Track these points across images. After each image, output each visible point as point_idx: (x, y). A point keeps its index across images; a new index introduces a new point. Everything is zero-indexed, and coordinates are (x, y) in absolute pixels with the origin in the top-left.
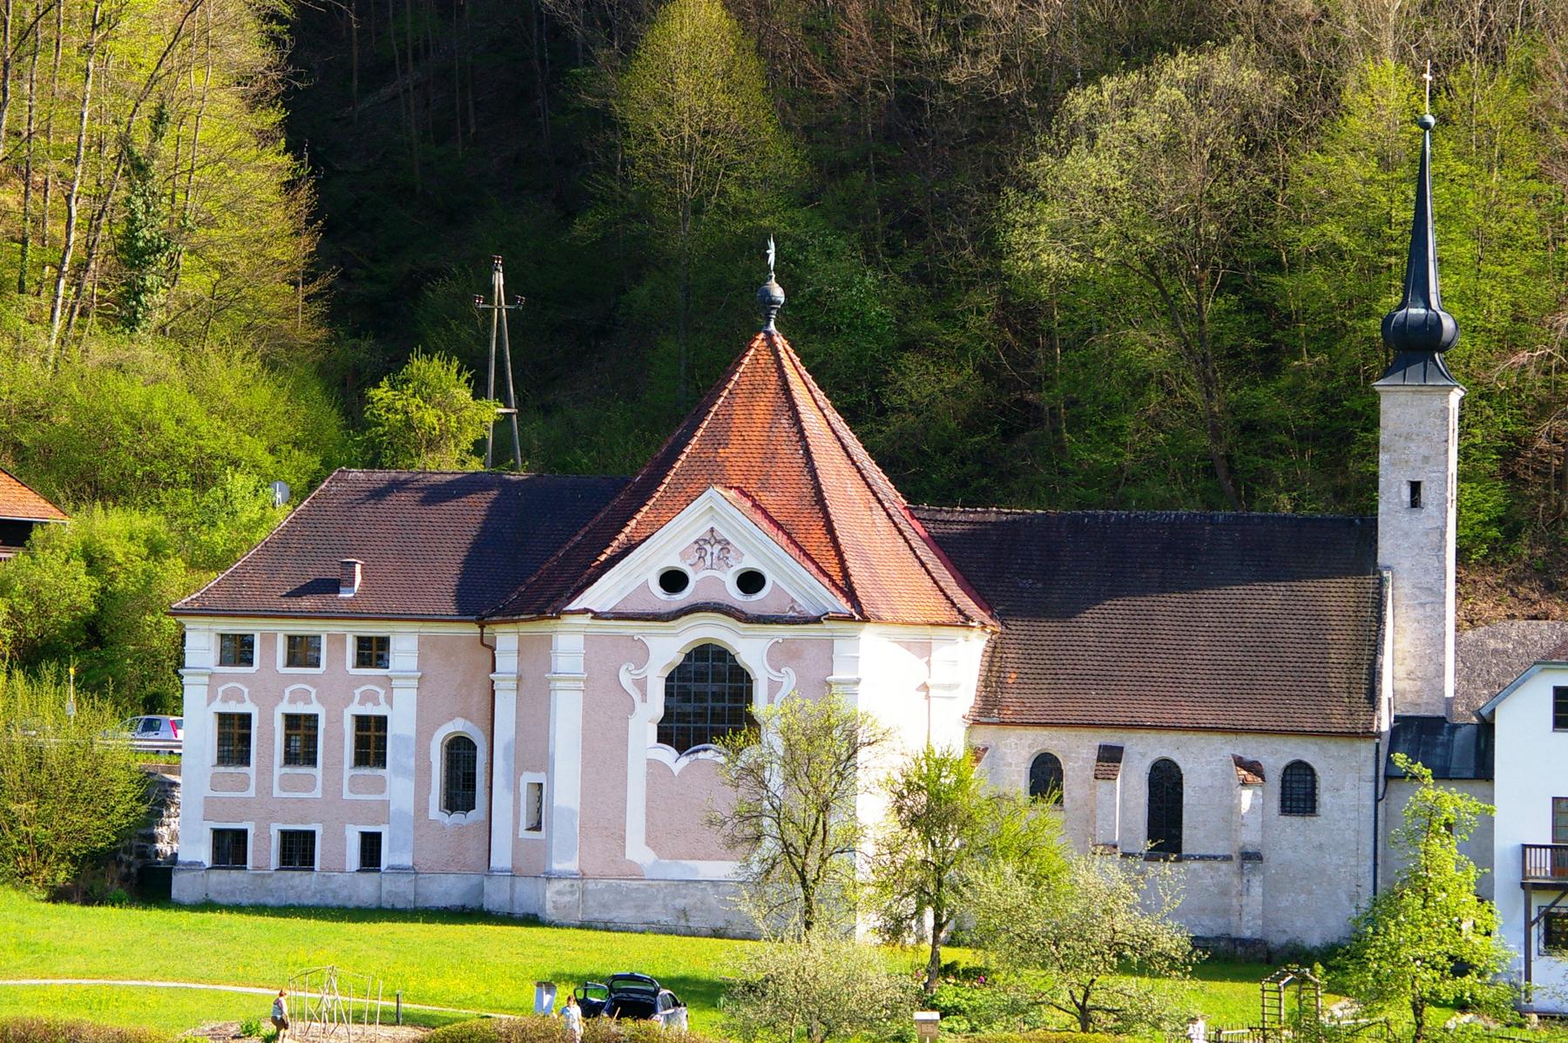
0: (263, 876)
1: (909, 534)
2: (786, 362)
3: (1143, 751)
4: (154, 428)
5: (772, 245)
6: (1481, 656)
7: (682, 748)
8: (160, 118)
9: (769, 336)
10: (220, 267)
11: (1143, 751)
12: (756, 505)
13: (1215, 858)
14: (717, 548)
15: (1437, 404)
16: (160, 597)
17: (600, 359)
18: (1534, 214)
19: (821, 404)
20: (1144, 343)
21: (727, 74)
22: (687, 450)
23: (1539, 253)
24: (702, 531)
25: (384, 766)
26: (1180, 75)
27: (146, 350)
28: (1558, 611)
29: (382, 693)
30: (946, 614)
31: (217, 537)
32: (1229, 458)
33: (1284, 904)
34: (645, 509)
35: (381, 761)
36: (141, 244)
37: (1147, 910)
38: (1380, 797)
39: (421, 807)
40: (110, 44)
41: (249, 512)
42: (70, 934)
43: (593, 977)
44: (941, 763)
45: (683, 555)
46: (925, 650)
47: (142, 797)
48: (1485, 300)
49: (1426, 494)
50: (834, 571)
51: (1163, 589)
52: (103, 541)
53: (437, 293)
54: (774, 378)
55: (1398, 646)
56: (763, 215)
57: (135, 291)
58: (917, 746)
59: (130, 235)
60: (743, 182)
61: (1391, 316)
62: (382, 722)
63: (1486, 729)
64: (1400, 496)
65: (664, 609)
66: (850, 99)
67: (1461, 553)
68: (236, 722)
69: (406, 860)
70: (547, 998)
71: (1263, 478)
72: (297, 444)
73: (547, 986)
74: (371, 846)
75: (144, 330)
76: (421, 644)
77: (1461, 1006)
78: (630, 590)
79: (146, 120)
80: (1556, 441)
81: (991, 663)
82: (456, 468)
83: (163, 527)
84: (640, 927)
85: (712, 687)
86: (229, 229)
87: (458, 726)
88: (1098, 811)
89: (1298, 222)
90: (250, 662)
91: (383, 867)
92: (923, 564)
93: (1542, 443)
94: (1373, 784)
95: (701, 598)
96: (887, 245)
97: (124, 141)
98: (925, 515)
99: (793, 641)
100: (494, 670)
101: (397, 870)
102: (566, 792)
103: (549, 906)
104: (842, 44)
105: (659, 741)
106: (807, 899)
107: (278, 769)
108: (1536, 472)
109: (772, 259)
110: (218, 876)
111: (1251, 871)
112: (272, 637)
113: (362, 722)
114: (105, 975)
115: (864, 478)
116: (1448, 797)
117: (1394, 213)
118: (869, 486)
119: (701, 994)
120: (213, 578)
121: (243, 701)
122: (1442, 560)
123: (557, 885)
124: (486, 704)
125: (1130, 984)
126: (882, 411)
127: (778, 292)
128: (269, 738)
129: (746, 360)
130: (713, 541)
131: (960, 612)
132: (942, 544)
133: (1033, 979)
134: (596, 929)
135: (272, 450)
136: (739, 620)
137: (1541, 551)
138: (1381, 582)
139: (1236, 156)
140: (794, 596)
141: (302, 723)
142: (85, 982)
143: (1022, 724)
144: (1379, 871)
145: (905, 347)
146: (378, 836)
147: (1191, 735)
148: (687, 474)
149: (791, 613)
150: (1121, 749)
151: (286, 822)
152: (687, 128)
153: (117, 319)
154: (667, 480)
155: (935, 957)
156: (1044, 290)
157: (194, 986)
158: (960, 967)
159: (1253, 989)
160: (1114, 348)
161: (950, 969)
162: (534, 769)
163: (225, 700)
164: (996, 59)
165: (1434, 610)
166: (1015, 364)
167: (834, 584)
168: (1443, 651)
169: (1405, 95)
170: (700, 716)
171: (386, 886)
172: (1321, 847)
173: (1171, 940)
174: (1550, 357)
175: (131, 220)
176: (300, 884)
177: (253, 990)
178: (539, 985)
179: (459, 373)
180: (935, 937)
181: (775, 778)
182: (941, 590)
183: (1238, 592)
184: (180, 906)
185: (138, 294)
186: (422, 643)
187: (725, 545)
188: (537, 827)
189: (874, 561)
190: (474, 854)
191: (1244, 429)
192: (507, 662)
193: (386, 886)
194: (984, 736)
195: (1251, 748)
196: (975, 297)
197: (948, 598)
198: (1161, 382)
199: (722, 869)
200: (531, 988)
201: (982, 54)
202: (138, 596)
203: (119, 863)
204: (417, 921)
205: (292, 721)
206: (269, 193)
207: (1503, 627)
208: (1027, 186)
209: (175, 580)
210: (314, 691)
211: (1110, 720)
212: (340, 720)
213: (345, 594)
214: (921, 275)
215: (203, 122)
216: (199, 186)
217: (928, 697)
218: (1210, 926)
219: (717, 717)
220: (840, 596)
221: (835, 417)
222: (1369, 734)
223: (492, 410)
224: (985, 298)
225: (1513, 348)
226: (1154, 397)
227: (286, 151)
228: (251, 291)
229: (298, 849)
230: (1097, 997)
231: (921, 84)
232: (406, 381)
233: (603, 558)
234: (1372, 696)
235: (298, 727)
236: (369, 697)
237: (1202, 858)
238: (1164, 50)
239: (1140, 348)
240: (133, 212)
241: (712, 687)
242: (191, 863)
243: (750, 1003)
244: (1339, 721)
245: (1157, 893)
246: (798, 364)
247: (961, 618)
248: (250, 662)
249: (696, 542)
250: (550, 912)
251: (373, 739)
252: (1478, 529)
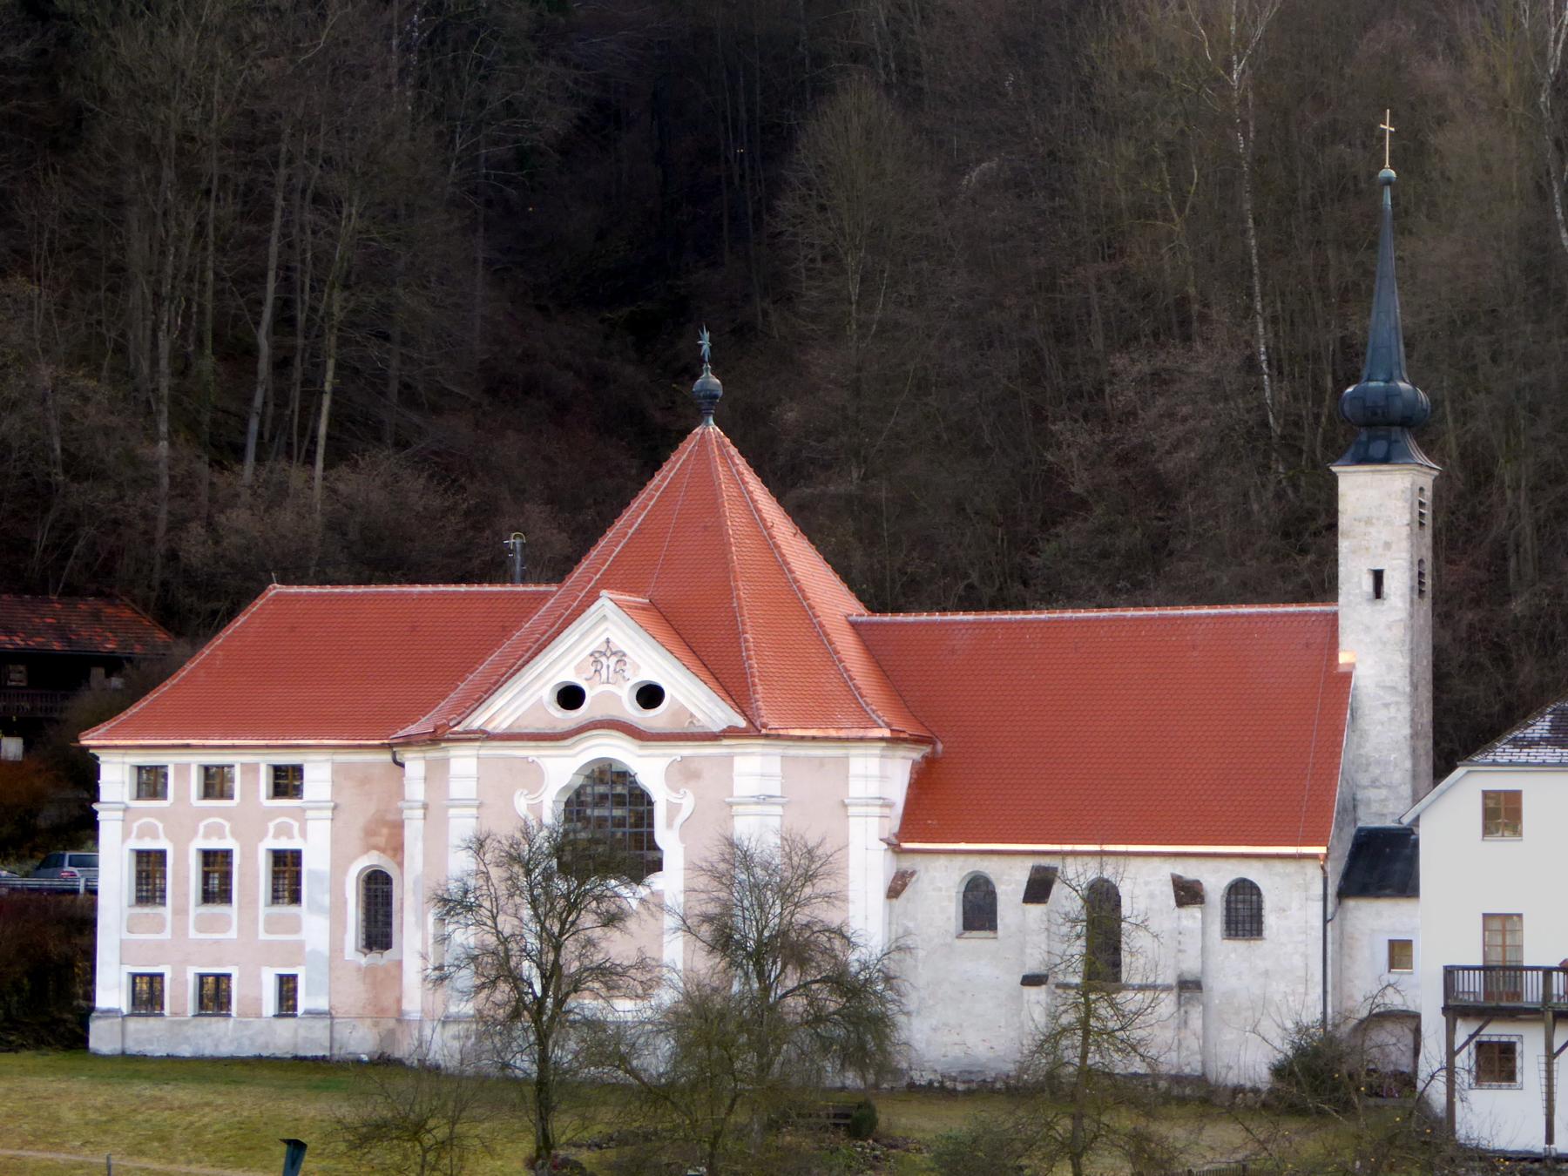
5: (707, 335)
14: (614, 659)
29: (296, 825)
38: (1329, 917)
39: (336, 948)
62: (296, 856)
64: (1360, 586)
69: (322, 1004)
74: (287, 987)
87: (372, 860)
91: (300, 1011)
94: (1321, 903)
95: (599, 714)
101: (313, 1014)
107: (195, 909)
110: (134, 1025)
128: (184, 876)
130: (608, 654)
144: (1329, 998)
151: (202, 966)
163: (140, 836)
165: (1398, 710)
172: (1266, 973)
186: (339, 771)
187: (621, 657)
193: (302, 1032)
236: (282, 831)
249: (592, 655)
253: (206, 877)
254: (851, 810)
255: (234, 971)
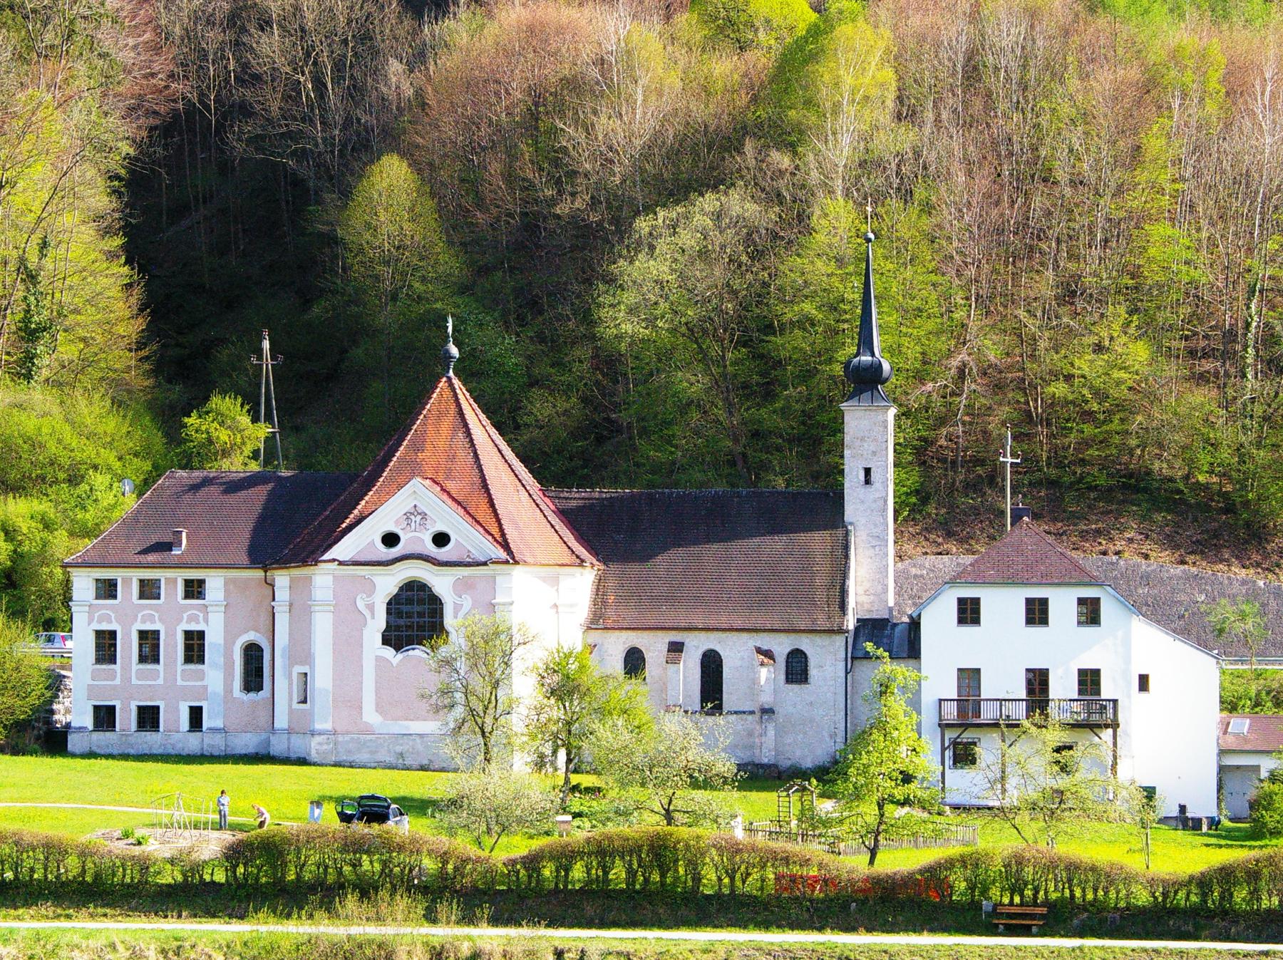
0: (127, 735)
1: (543, 507)
2: (460, 396)
3: (697, 645)
4: (42, 446)
6: (907, 579)
7: (398, 648)
8: (44, 245)
9: (449, 379)
10: (84, 340)
11: (697, 645)
12: (443, 490)
13: (744, 712)
15: (880, 418)
16: (52, 555)
17: (330, 396)
18: (934, 296)
19: (484, 423)
20: (688, 381)
21: (412, 210)
22: (398, 454)
23: (938, 320)
24: (409, 507)
25: (203, 663)
26: (708, 208)
27: (37, 395)
28: (954, 550)
30: (568, 558)
31: (88, 516)
32: (744, 455)
33: (789, 741)
34: (371, 493)
35: (201, 660)
36: (33, 326)
37: (707, 747)
40: (10, 197)
41: (107, 499)
42: (5, 774)
43: (345, 798)
44: (568, 656)
45: (397, 522)
46: (555, 581)
47: (50, 685)
48: (904, 350)
49: (874, 476)
50: (495, 531)
51: (708, 540)
52: (14, 519)
53: (224, 355)
54: (453, 407)
55: (858, 574)
56: (437, 300)
57: (30, 357)
58: (553, 646)
59: (27, 319)
60: (424, 280)
61: (849, 362)
62: (201, 635)
63: (915, 625)
65: (384, 558)
66: (491, 225)
67: (897, 513)
68: (107, 636)
70: (317, 811)
71: (764, 467)
72: (136, 455)
73: (318, 803)
74: (196, 716)
75: (36, 381)
76: (226, 584)
77: (905, 802)
78: (361, 547)
79: (35, 246)
80: (951, 440)
81: (598, 590)
82: (241, 468)
83: (52, 510)
84: (373, 765)
85: (417, 608)
86: (89, 316)
87: (251, 636)
88: (669, 684)
89: (784, 301)
90: (115, 597)
91: (204, 729)
92: (553, 526)
93: (943, 442)
95: (408, 551)
96: (518, 319)
97: (22, 260)
98: (553, 494)
99: (469, 577)
100: (274, 600)
101: (213, 730)
102: (323, 679)
103: (313, 752)
104: (485, 189)
105: (383, 644)
106: (485, 745)
108: (939, 460)
109: (450, 330)
111: (767, 720)
112: (128, 580)
113: (189, 635)
114: (30, 800)
115: (513, 471)
116: (899, 669)
117: (846, 296)
118: (516, 476)
119: (416, 807)
120: (88, 543)
121: (111, 622)
122: (885, 518)
123: (318, 739)
124: (269, 622)
125: (700, 795)
126: (517, 427)
127: (454, 351)
128: (128, 647)
129: (435, 395)
131: (578, 557)
132: (563, 514)
133: (635, 793)
134: (344, 766)
135: (120, 459)
136: (434, 564)
137: (943, 511)
138: (847, 533)
139: (744, 258)
140: (470, 548)
141: (150, 636)
142: (18, 804)
143: (619, 629)
145: (531, 385)
146: (200, 708)
147: (728, 634)
148: (397, 470)
149: (468, 560)
150: (682, 644)
152: (386, 245)
153: (19, 375)
154: (385, 474)
155: (567, 781)
156: (623, 347)
157: (88, 806)
158: (582, 787)
159: (775, 794)
160: (668, 384)
161: (575, 788)
162: (302, 663)
164: (587, 198)
166: (604, 396)
167: (496, 540)
168: (887, 576)
169: (850, 220)
170: (409, 627)
171: (207, 741)
173: (725, 766)
174: (946, 386)
175: (28, 311)
176: (150, 740)
177: (125, 809)
178: (312, 803)
179: (242, 406)
180: (567, 768)
181: (462, 665)
182: (565, 543)
183: (757, 540)
184: (74, 755)
185: (32, 358)
186: (227, 582)
187: (424, 516)
188: (305, 701)
189: (521, 525)
190: (263, 719)
191: (753, 435)
192: (282, 594)
194: (595, 636)
195: (766, 641)
196: (578, 352)
197: (569, 548)
198: (699, 406)
199: (430, 726)
200: (306, 807)
201: (578, 195)
202: (38, 555)
203: (34, 728)
204: (228, 763)
205: (143, 635)
206: (115, 292)
207: (921, 560)
208: (610, 280)
209: (61, 543)
210: (113, 615)
211: (676, 625)
212: (174, 634)
213: (176, 552)
214: (541, 338)
215: (73, 246)
216: (71, 288)
217: (557, 612)
218: (745, 756)
219: (421, 627)
220: (499, 547)
221: (493, 431)
222: (841, 631)
223: (263, 430)
224: (583, 352)
225: (922, 381)
226: (695, 415)
227: (126, 263)
228: (104, 355)
229: (148, 717)
230: (678, 803)
231: (537, 215)
232: (207, 413)
233: (344, 526)
234: (843, 607)
235: (147, 639)
236: (192, 619)
237: (736, 713)
238: (695, 191)
239: (685, 384)
240: (28, 306)
241: (417, 608)
242: (80, 728)
243: (452, 812)
244: (822, 623)
245: (714, 735)
246: (468, 397)
247: (578, 561)
248: (115, 597)
250: (314, 756)
251: (196, 646)
252: (903, 498)
253: (140, 645)
254: (209, 609)
255: (118, 704)
